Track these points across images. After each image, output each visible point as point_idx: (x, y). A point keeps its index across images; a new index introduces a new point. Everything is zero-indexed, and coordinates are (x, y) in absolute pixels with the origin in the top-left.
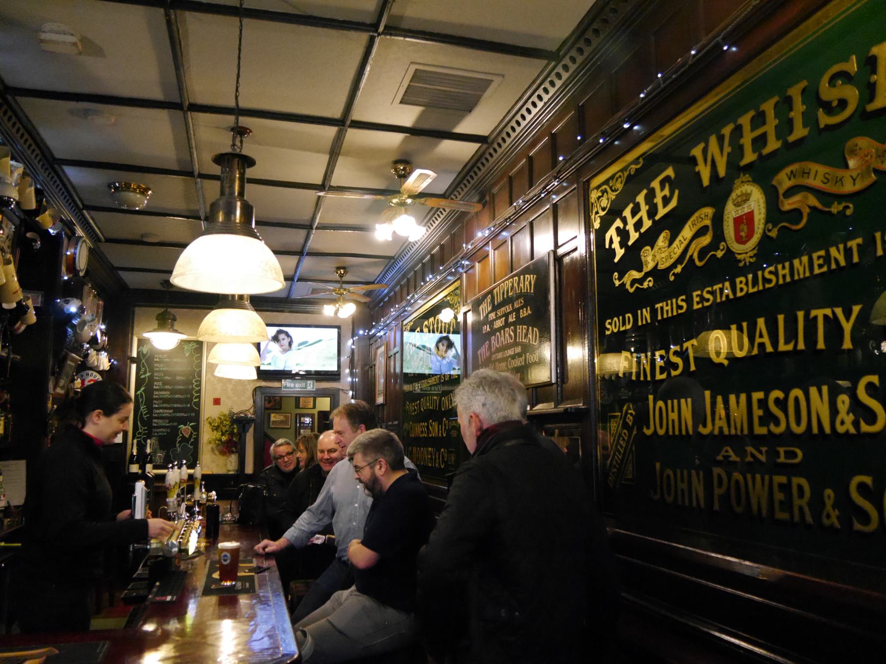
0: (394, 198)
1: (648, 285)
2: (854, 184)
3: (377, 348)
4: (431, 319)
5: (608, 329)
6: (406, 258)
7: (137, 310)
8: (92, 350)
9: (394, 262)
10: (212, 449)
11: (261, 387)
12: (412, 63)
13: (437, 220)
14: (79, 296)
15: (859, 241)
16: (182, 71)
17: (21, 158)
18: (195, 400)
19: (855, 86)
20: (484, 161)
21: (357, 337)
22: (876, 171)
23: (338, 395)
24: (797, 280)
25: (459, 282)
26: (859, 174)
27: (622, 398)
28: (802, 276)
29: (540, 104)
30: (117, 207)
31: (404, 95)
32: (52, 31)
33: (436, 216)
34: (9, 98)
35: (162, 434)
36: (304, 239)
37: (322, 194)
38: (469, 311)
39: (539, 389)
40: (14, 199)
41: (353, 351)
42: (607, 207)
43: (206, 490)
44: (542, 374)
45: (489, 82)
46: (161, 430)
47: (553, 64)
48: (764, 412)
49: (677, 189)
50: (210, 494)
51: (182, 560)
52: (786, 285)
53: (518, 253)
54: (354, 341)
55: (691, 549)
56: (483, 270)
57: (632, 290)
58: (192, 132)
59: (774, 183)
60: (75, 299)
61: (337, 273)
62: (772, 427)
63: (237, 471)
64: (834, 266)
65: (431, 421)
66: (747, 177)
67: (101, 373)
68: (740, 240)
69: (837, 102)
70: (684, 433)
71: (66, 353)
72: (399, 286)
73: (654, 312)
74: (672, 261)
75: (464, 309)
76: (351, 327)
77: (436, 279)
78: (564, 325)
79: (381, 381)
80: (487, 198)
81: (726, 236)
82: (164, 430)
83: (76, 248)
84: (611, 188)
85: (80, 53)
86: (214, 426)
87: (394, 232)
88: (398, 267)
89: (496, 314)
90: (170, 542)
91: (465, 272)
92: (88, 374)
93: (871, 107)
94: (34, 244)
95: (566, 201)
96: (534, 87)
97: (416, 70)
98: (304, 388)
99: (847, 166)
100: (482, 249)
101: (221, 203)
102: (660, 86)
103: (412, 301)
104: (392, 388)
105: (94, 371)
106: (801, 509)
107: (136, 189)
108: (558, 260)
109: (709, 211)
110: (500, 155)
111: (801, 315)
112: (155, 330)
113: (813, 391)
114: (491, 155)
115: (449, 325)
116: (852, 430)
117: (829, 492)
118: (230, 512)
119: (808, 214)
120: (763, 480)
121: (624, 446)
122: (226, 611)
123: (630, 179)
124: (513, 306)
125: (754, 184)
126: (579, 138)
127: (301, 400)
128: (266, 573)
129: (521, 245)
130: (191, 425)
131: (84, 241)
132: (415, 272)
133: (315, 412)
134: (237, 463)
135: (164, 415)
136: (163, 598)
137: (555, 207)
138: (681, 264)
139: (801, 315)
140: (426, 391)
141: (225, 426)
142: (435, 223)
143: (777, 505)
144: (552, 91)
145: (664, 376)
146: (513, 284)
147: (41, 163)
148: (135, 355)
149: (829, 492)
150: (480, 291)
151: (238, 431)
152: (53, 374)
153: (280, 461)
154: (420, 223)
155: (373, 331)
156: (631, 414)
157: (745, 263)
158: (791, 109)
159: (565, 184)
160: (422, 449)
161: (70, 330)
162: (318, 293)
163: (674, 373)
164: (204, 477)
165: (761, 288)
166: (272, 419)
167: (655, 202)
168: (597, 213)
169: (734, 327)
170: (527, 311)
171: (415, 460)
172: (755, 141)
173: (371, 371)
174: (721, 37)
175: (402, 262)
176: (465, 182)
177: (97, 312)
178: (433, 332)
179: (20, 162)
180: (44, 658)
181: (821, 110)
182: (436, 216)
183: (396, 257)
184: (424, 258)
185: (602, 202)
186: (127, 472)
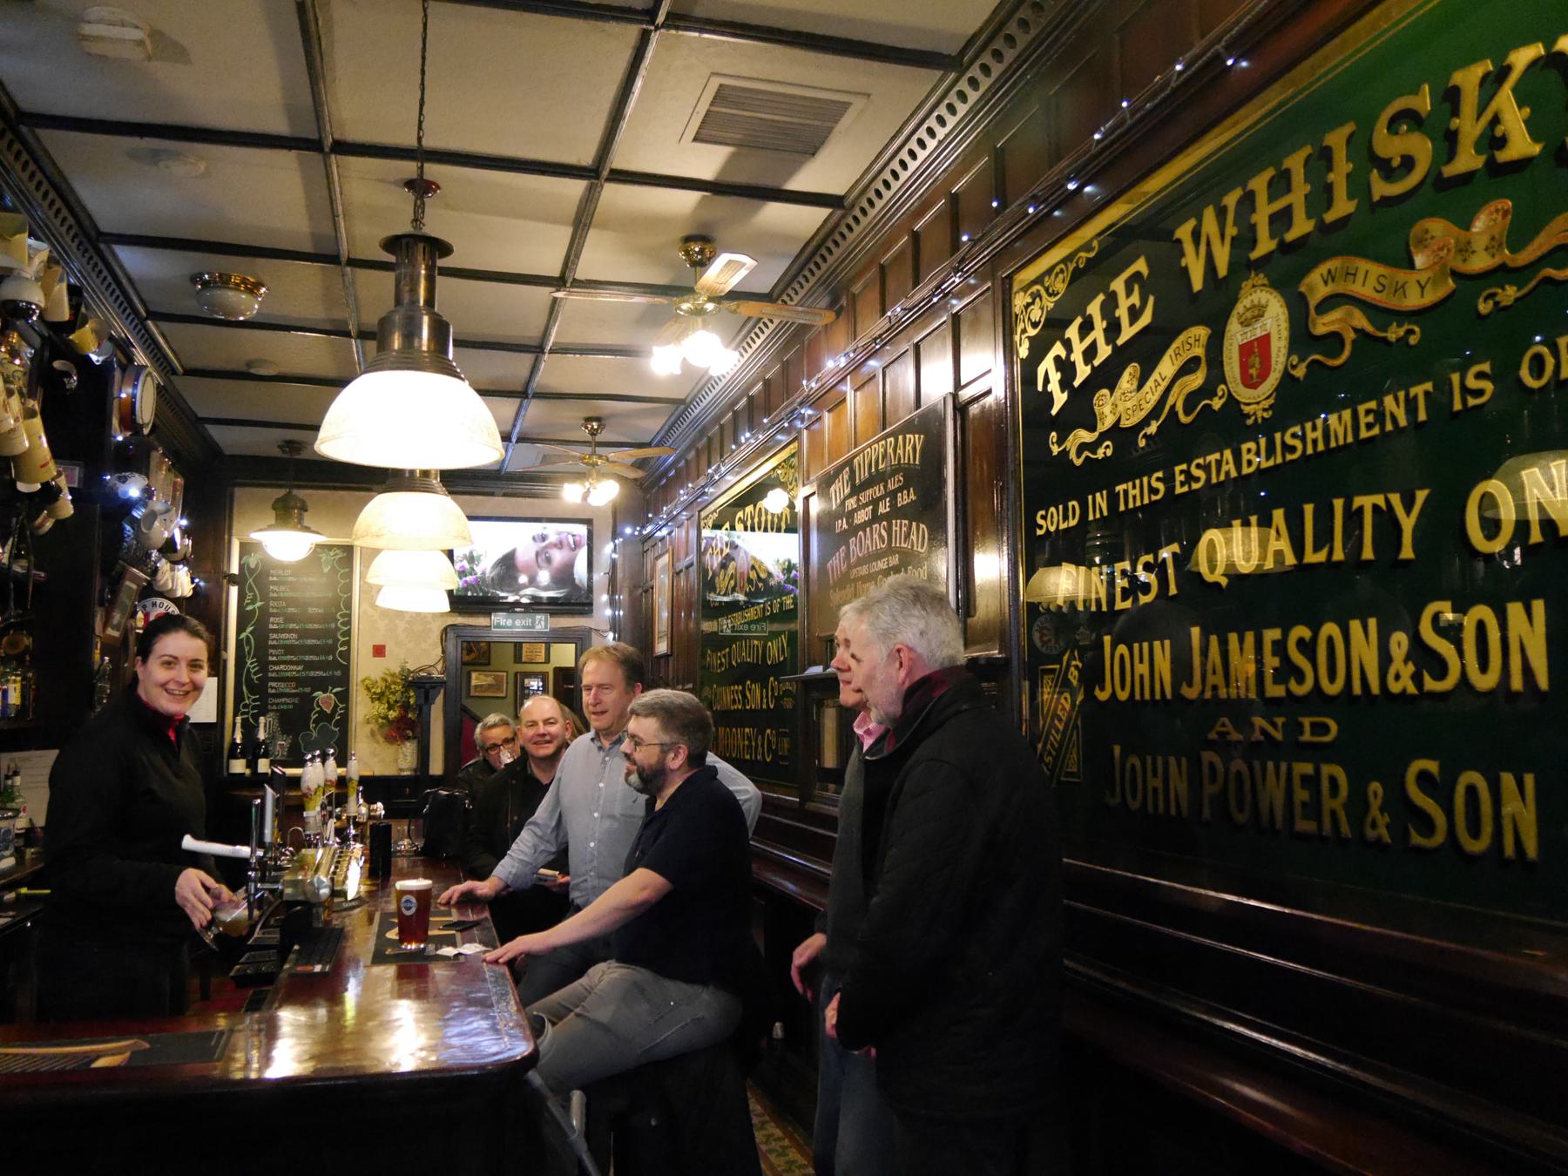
0: (684, 302)
1: (1105, 453)
2: (1422, 296)
3: (657, 558)
4: (749, 509)
5: (1041, 527)
7: (238, 491)
8: (164, 561)
9: (686, 409)
10: (373, 734)
11: (454, 625)
12: (713, 74)
13: (759, 337)
14: (144, 470)
16: (322, 86)
17: (45, 234)
20: (845, 231)
21: (621, 540)
22: (1455, 274)
25: (795, 444)
26: (1429, 278)
27: (1081, 643)
28: (1341, 442)
29: (931, 144)
30: (207, 315)
32: (100, 21)
34: (24, 129)
35: (285, 707)
37: (560, 295)
38: (814, 494)
40: (37, 305)
41: (614, 563)
42: (1040, 321)
43: (365, 801)
45: (846, 105)
46: (283, 700)
47: (953, 76)
48: (1281, 662)
49: (1153, 294)
51: (334, 912)
52: (1317, 454)
54: (615, 546)
55: (1166, 883)
56: (837, 424)
57: (1078, 462)
58: (338, 189)
59: (1302, 289)
60: (137, 475)
61: (586, 428)
62: (1293, 686)
63: (415, 770)
64: (1389, 427)
65: (749, 682)
66: (1261, 279)
67: (178, 601)
68: (1249, 382)
69: (1399, 159)
70: (1158, 697)
71: (124, 567)
73: (1113, 499)
74: (1143, 414)
75: (806, 491)
76: (611, 521)
77: (757, 439)
79: (663, 616)
80: (844, 302)
81: (1229, 378)
83: (135, 387)
84: (1047, 290)
85: (149, 58)
86: (375, 693)
87: (685, 359)
89: (858, 500)
90: (315, 880)
91: (806, 428)
92: (154, 604)
93: (1450, 170)
94: (65, 380)
95: (975, 310)
96: (921, 114)
97: (721, 85)
98: (529, 627)
101: (397, 318)
102: (1126, 121)
103: (717, 477)
104: (682, 626)
107: (238, 285)
108: (961, 409)
109: (1201, 332)
111: (1338, 504)
112: (270, 528)
113: (1355, 625)
114: (850, 228)
116: (1412, 689)
117: (1375, 786)
119: (1354, 342)
120: (1277, 768)
121: (1064, 718)
122: (412, 987)
123: (1077, 275)
124: (885, 487)
125: (1272, 290)
126: (995, 204)
129: (900, 384)
131: (149, 374)
132: (722, 427)
133: (549, 668)
134: (415, 756)
135: (289, 674)
136: (309, 968)
137: (956, 318)
138: (1157, 421)
139: (1338, 504)
140: (741, 631)
142: (754, 342)
144: (951, 121)
145: (1128, 604)
146: (886, 450)
149: (1375, 786)
150: (831, 460)
151: (416, 701)
152: (101, 604)
155: (649, 529)
156: (1076, 667)
157: (1256, 419)
158: (1330, 168)
159: (972, 281)
160: (734, 730)
161: (128, 528)
162: (553, 463)
163: (1144, 599)
164: (363, 780)
165: (1279, 460)
166: (474, 682)
167: (1117, 315)
168: (1024, 331)
170: (908, 495)
171: (721, 749)
172: (1092, 328)
173: (646, 598)
174: (1223, 43)
175: (699, 409)
177: (174, 498)
178: (753, 529)
179: (42, 241)
180: (128, 1054)
181: (1375, 171)
182: (757, 330)
184: (737, 403)
185: (1032, 311)
186: (225, 774)
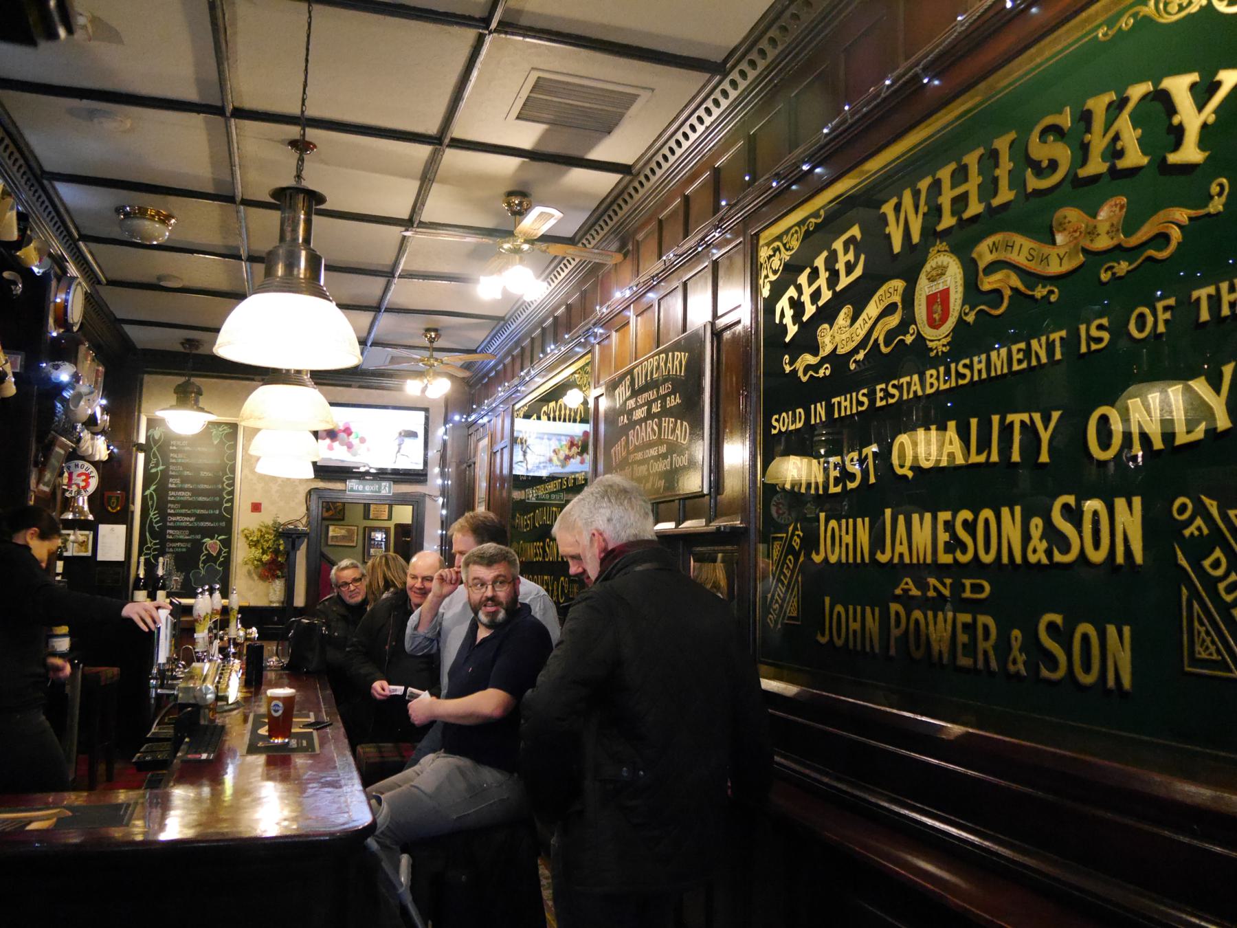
1: (824, 373)
2: (1061, 265)
3: (478, 441)
4: (552, 404)
5: (775, 428)
6: (520, 320)
7: (147, 378)
9: (505, 324)
10: (249, 573)
13: (563, 271)
15: (1063, 333)
16: (226, 66)
18: (225, 505)
19: (1069, 147)
20: (627, 198)
21: (451, 425)
22: (1085, 251)
23: (424, 502)
24: (993, 377)
25: (589, 356)
28: (999, 372)
29: (700, 129)
31: (522, 109)
33: (562, 265)
36: (382, 291)
39: (687, 502)
41: (445, 443)
42: (779, 269)
43: (243, 626)
44: (694, 482)
45: (636, 96)
46: (178, 544)
47: (718, 78)
50: (250, 631)
52: (981, 381)
53: (667, 322)
56: (622, 341)
57: (804, 379)
59: (974, 255)
60: (67, 364)
61: (426, 336)
62: (958, 554)
63: (283, 603)
66: (943, 246)
68: (933, 324)
70: (859, 560)
72: (510, 358)
73: (830, 409)
74: (854, 344)
76: (443, 410)
77: (560, 350)
78: (721, 419)
79: (482, 486)
80: (630, 247)
82: (182, 545)
83: (68, 293)
84: (785, 245)
88: (508, 332)
89: (637, 401)
91: (598, 343)
92: (77, 466)
94: (13, 287)
95: (730, 258)
96: (693, 106)
97: (539, 78)
98: (376, 492)
99: (1054, 243)
100: (620, 316)
101: (281, 251)
103: (527, 379)
105: (85, 460)
106: (985, 653)
107: (153, 216)
108: (717, 334)
109: (899, 284)
110: (648, 191)
111: (996, 419)
112: (172, 407)
113: (1005, 511)
114: (636, 190)
115: (576, 413)
116: (1045, 561)
117: (1016, 633)
118: (277, 655)
122: (278, 772)
123: (807, 234)
124: (658, 392)
126: (747, 178)
127: (372, 507)
128: (328, 730)
130: (220, 538)
133: (391, 525)
134: (283, 591)
135: (184, 524)
136: (198, 756)
137: (715, 264)
140: (543, 500)
141: (267, 541)
143: (959, 648)
145: (838, 489)
146: (659, 364)
147: (25, 177)
148: (142, 440)
152: (36, 464)
153: (343, 589)
154: (538, 277)
155: (473, 417)
156: (798, 536)
157: (937, 352)
159: (728, 236)
161: (59, 405)
163: (851, 486)
164: (242, 610)
166: (331, 534)
168: (767, 277)
169: (952, 425)
170: (675, 400)
172: (955, 201)
174: (921, 66)
175: (515, 325)
176: (601, 223)
177: (96, 382)
180: (55, 820)
181: (1030, 170)
182: (562, 265)
183: (507, 318)
185: (773, 263)
